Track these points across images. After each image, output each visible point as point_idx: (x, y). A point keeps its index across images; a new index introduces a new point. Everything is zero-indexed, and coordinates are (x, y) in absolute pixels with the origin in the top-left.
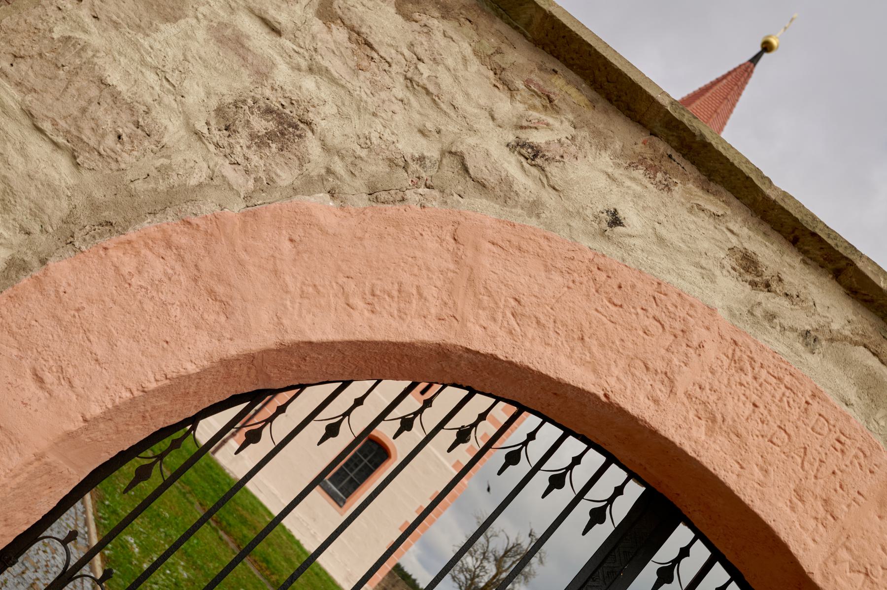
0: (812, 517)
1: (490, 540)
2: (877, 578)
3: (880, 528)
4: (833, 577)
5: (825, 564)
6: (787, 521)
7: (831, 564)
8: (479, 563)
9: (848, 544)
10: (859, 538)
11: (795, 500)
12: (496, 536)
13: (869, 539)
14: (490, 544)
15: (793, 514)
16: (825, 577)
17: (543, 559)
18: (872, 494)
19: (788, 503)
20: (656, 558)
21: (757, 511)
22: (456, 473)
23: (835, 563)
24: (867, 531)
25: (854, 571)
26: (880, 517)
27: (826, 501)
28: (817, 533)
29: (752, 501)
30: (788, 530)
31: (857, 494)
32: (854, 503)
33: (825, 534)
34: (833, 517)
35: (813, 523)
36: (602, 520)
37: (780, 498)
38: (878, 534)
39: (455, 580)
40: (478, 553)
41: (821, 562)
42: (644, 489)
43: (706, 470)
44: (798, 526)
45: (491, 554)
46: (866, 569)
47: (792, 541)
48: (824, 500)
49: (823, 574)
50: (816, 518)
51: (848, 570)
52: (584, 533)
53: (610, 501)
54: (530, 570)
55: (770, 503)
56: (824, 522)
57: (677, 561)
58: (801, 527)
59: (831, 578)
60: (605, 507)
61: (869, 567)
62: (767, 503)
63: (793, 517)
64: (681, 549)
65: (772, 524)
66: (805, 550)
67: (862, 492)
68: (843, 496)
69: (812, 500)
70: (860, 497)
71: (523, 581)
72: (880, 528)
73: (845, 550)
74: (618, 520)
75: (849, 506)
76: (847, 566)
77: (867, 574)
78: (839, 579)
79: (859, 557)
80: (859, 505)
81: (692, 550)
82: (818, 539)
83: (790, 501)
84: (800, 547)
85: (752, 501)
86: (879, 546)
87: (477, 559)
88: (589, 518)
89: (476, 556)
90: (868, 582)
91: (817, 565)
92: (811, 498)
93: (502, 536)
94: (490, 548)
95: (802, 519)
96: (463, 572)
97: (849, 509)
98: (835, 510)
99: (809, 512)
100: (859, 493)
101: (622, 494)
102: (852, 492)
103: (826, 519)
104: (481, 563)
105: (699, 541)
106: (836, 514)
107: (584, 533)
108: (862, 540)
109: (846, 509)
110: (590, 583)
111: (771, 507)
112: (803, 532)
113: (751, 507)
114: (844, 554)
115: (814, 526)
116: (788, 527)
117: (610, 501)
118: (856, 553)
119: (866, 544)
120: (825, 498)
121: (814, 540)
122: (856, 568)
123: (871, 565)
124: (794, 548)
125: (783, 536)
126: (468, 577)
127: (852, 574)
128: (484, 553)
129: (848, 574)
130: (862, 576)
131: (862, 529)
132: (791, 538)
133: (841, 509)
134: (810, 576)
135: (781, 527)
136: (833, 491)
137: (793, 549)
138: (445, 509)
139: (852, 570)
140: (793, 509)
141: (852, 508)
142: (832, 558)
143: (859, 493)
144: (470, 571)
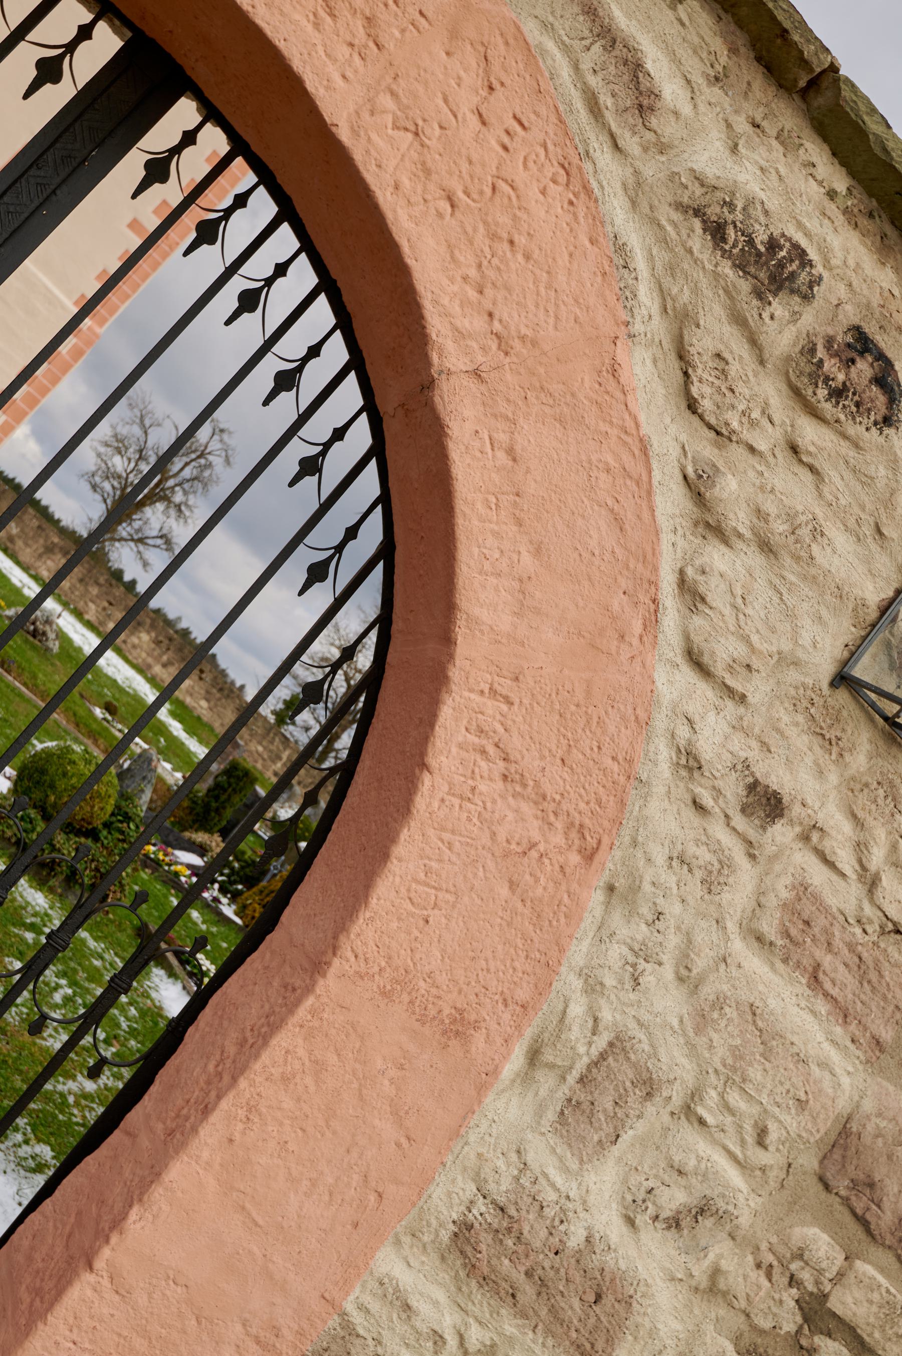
0: (345, 42)
1: (149, 431)
2: (429, 139)
3: (446, 68)
4: (366, 131)
5: (357, 113)
6: (305, 42)
7: (366, 115)
8: (132, 465)
9: (394, 87)
10: (412, 80)
11: (322, 13)
12: (159, 425)
13: (426, 84)
14: (149, 437)
15: (317, 34)
16: (355, 132)
17: (231, 459)
18: (441, 17)
19: (311, 17)
20: (144, 143)
21: (259, 22)
22: (75, 310)
23: (372, 113)
24: (425, 71)
25: (398, 128)
26: (448, 54)
27: (369, 20)
28: (350, 66)
29: (253, 7)
30: (306, 56)
31: (418, 15)
32: (411, 27)
33: (361, 69)
34: (377, 45)
35: (346, 50)
36: (56, 78)
37: (298, 6)
38: (441, 77)
39: (95, 491)
40: (131, 450)
41: (351, 110)
42: (323, 294)
43: (386, 225)
44: (322, 54)
45: (150, 453)
46: (417, 125)
47: (310, 74)
48: (367, 18)
49: (352, 128)
50: (351, 45)
51: (390, 125)
52: (26, 96)
53: (70, 47)
54: (211, 475)
55: (282, 13)
56: (363, 50)
57: (176, 150)
58: (327, 55)
59: (362, 133)
60: (61, 57)
61: (420, 123)
62: (276, 12)
63: (316, 38)
64: (184, 132)
65: (281, 45)
66: (327, 88)
67: (425, 12)
68: (396, 15)
69: (349, 16)
70: (423, 20)
71: (200, 490)
72: (446, 68)
73: (388, 97)
74: (83, 80)
75: (403, 31)
76: (389, 119)
77: (417, 134)
78: (374, 136)
79: (408, 107)
80: (419, 31)
81: (200, 136)
82: (349, 74)
83: (315, 15)
84: (321, 83)
85: (253, 7)
86: (440, 95)
87: (129, 460)
88: (35, 73)
89: (128, 454)
90: (416, 144)
91: (345, 115)
92: (346, 13)
93: (168, 424)
94: (150, 444)
95: (328, 43)
96: (107, 478)
97: (403, 35)
98: (381, 34)
99: (341, 33)
100: (421, 13)
101: (90, 38)
102: (410, 9)
103: (366, 46)
104: (136, 465)
105: (239, 161)
106: (382, 40)
107: (26, 96)
108: (416, 83)
109: (397, 34)
110: (33, 172)
111: (282, 19)
112: (328, 62)
113: (251, 15)
114: (386, 101)
115: (347, 56)
116: (305, 52)
117: (70, 47)
118: (405, 101)
119: (421, 90)
120: (368, 15)
121: (344, 77)
122: (402, 123)
123: (424, 120)
124: (312, 84)
125: (297, 64)
126: (116, 484)
127: (396, 131)
128: (141, 451)
129: (390, 131)
130: (410, 136)
131: (419, 67)
132: (308, 68)
133: (391, 35)
134: (334, 129)
135: (295, 51)
136: (381, 6)
137: (310, 86)
138: (66, 368)
139: (396, 127)
140: (317, 26)
141: (407, 34)
142: (368, 106)
143: (421, 13)
144: (119, 477)
